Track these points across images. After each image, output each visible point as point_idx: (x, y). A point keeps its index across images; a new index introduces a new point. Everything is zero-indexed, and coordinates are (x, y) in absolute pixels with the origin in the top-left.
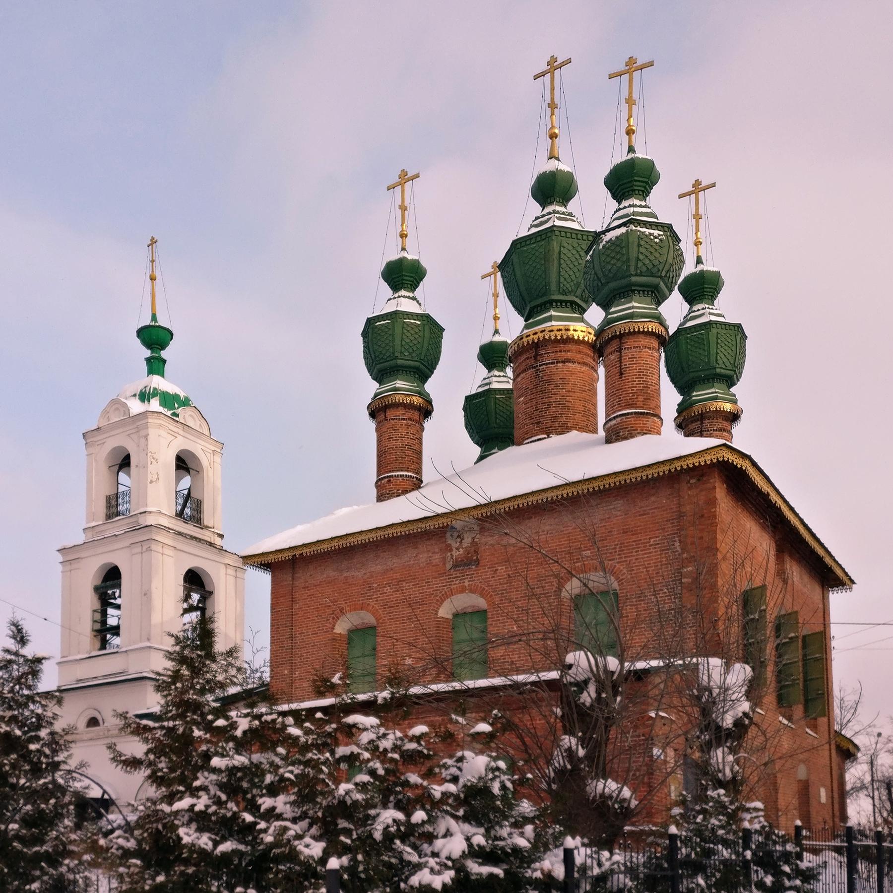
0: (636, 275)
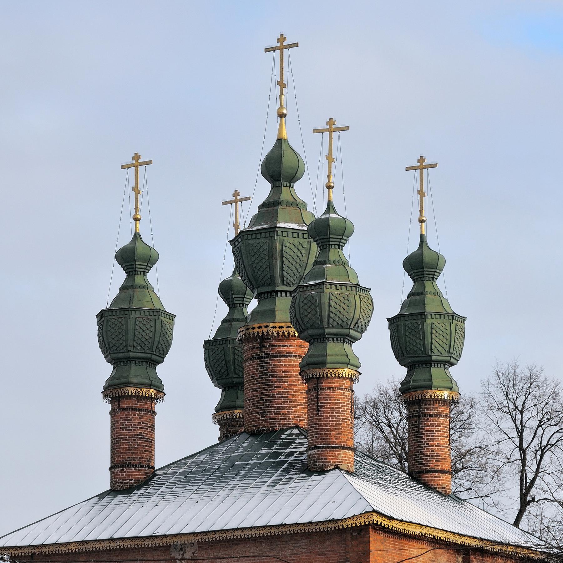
0: (329, 327)
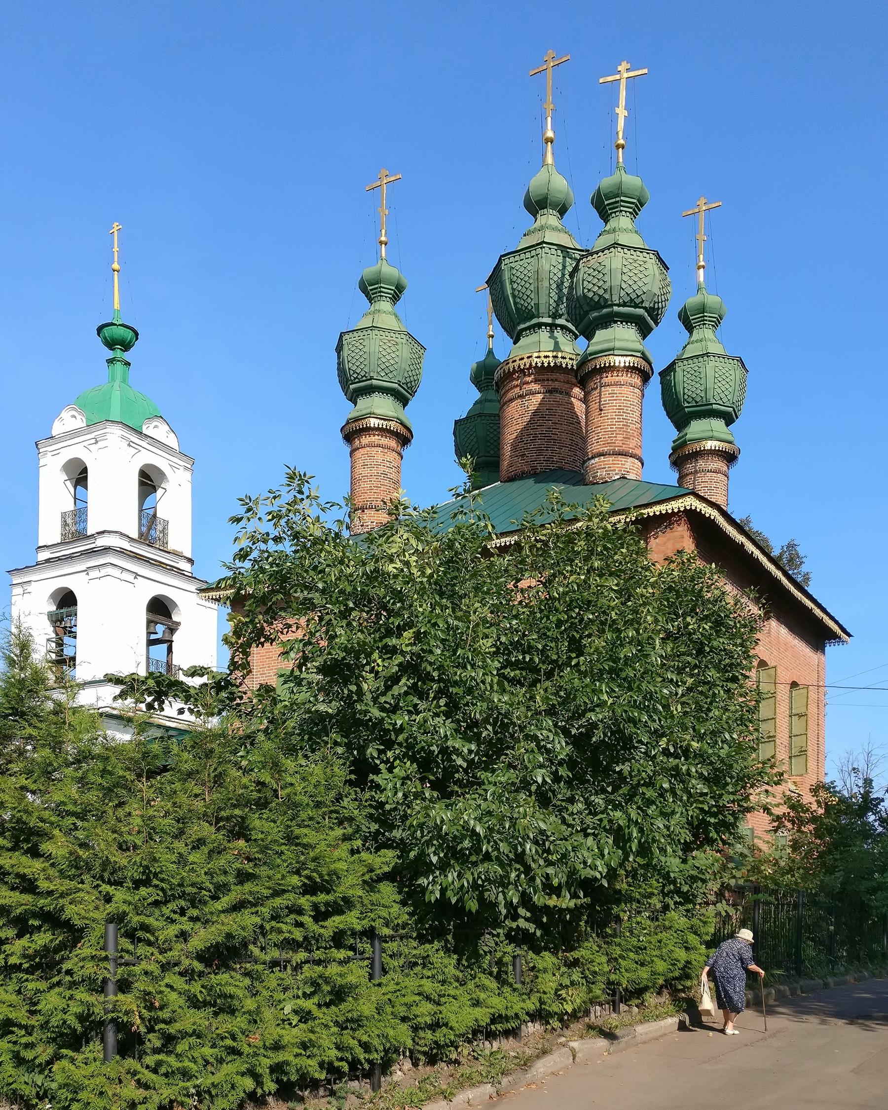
0: (619, 305)
